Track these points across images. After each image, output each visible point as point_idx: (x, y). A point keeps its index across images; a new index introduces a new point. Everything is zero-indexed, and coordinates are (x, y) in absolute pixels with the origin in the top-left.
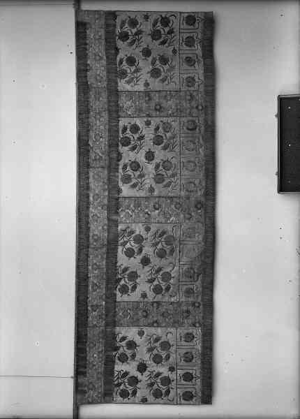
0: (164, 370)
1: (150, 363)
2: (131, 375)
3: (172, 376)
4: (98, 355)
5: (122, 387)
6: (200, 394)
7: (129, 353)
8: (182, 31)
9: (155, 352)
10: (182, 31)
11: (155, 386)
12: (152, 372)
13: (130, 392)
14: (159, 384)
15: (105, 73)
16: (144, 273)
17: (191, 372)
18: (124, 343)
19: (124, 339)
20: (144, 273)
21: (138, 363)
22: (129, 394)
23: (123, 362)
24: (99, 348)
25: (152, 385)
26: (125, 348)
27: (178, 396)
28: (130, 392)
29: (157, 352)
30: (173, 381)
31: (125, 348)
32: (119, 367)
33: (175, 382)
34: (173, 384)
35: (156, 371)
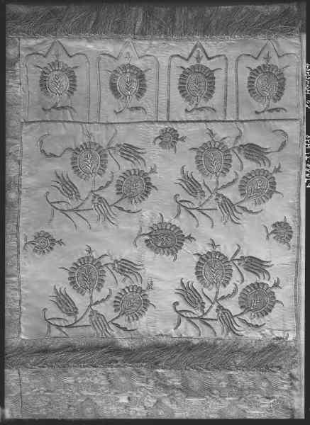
0: (167, 169)
1: (151, 212)
2: (191, 278)
3: (193, 134)
4: (123, 391)
5: (233, 307)
6: (261, 40)
7: (113, 284)
8: (93, 114)
9: (110, 195)
10: (93, 114)
11: (232, 194)
12: (180, 203)
13: (251, 279)
14: (223, 180)
15: (267, 344)
16: (211, 232)
17: (176, 73)
18: (80, 301)
19: (63, 301)
20: (211, 232)
21: (149, 255)
22: (256, 286)
23: (146, 303)
24: (95, 387)
25: (228, 207)
26: (97, 296)
27: (267, 115)
28: (251, 279)
29: (112, 189)
30: (211, 133)
31: (97, 296)
32: (158, 322)
33: (216, 128)
34: (220, 132)
35: (179, 190)
